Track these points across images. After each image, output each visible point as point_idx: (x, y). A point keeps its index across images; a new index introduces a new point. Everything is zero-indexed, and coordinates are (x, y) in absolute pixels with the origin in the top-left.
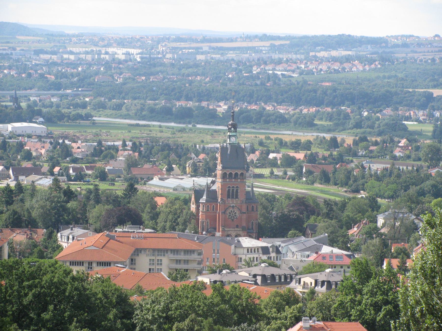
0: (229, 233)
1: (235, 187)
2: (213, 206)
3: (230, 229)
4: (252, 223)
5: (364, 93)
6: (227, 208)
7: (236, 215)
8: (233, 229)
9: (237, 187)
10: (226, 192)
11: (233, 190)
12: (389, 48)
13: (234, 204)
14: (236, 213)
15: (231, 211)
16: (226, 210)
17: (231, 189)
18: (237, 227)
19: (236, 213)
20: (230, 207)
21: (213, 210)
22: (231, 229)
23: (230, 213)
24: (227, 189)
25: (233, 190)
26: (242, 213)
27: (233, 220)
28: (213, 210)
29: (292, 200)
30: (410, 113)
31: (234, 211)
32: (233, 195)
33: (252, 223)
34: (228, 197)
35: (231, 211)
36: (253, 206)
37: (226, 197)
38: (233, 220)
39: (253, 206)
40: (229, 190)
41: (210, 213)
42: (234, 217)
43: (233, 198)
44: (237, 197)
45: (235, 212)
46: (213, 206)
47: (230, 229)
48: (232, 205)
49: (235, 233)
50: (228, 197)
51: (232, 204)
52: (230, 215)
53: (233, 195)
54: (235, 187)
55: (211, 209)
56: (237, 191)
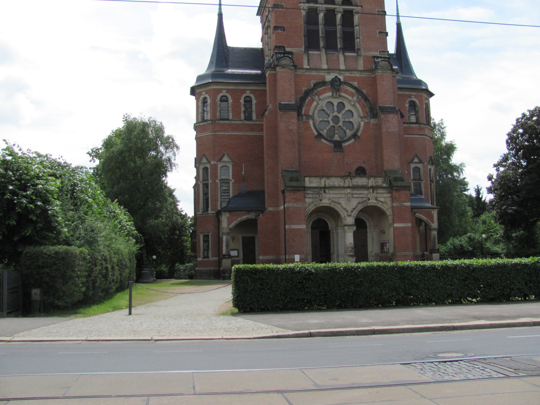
0: (325, 202)
2: (248, 101)
5: (2, 316)
6: (308, 93)
10: (301, 21)
12: (248, 90)
16: (303, 99)
18: (361, 172)
20: (324, 83)
21: (248, 118)
22: (336, 182)
26: (374, 110)
28: (248, 118)
29: (113, 149)
31: (341, 106)
32: (330, 37)
34: (312, 43)
37: (302, 40)
38: (338, 145)
40: (312, 14)
41: (236, 128)
43: (331, 46)
44: (349, 44)
45: (348, 107)
46: (248, 101)
48: (329, 77)
49: (354, 202)
50: (312, 43)
51: (329, 70)
53: (330, 37)
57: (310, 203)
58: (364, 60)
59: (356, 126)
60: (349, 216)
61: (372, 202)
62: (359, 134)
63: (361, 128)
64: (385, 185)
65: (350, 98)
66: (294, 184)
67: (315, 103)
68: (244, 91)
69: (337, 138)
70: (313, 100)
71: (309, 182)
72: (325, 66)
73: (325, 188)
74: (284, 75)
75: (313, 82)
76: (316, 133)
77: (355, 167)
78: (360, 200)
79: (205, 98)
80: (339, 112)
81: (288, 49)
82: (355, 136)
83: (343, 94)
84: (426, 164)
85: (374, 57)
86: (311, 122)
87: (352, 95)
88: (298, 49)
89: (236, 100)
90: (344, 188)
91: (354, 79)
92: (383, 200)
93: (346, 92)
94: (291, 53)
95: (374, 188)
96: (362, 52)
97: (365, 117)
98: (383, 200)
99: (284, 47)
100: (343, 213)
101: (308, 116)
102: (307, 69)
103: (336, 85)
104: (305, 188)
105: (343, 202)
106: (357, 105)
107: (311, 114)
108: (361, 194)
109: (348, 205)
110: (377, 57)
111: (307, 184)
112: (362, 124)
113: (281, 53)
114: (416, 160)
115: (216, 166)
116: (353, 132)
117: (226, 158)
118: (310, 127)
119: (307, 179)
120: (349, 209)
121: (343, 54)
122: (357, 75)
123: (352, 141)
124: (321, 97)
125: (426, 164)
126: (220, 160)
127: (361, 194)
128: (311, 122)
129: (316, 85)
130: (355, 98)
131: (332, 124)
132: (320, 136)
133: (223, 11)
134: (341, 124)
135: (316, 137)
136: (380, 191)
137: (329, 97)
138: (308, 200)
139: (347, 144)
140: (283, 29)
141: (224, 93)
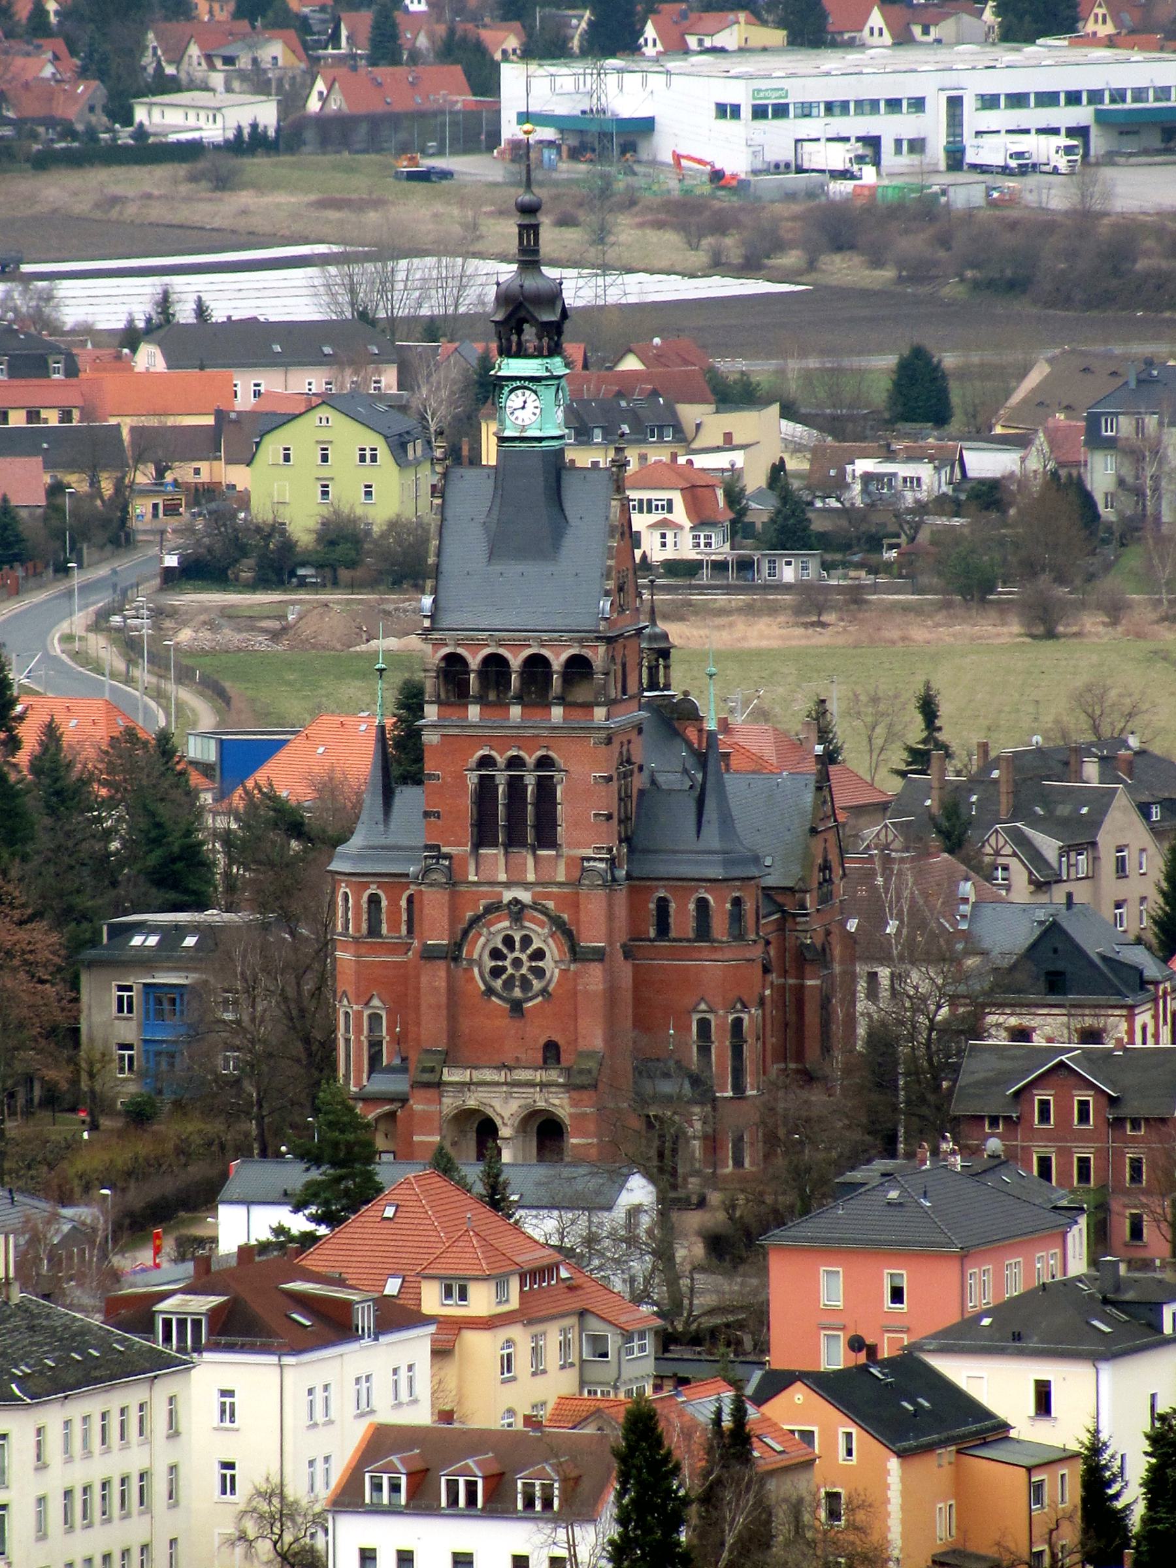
0: (472, 1103)
1: (530, 760)
3: (478, 1075)
4: (704, 1025)
6: (465, 933)
7: (540, 973)
8: (500, 1077)
9: (545, 763)
11: (516, 785)
13: (526, 885)
14: (539, 955)
15: (509, 941)
17: (501, 778)
19: (539, 955)
22: (489, 1075)
23: (496, 954)
24: (472, 779)
25: (516, 785)
26: (576, 953)
27: (517, 1007)
30: (572, 1546)
31: (526, 941)
33: (704, 1025)
34: (483, 836)
35: (509, 941)
36: (702, 904)
38: (517, 1007)
39: (702, 904)
40: (486, 786)
41: (393, 948)
42: (526, 984)
43: (514, 840)
44: (546, 836)
47: (478, 1075)
48: (508, 896)
50: (483, 836)
51: (508, 885)
52: (497, 972)
54: (530, 760)
55: (394, 926)
56: (546, 788)
57: (450, 1103)
58: (567, 865)
59: (548, 975)
60: (505, 1124)
61: (541, 1104)
62: (550, 989)
63: (555, 980)
64: (561, 1080)
65: (539, 930)
66: (426, 1077)
67: (482, 940)
68: (696, 890)
69: (517, 993)
70: (480, 935)
71: (451, 1075)
72: (503, 877)
73: (471, 1083)
74: (435, 904)
75: (482, 903)
76: (483, 987)
77: (542, 1041)
78: (522, 1102)
79: (346, 894)
80: (523, 950)
81: (444, 850)
82: (544, 991)
83: (527, 924)
84: (721, 1012)
85: (584, 859)
86: (476, 970)
87: (541, 925)
88: (460, 850)
89: (394, 902)
90: (497, 1084)
91: (548, 896)
92: (557, 1102)
93: (533, 920)
94: (448, 857)
95: (543, 1085)
96: (565, 851)
97: (562, 961)
98: (560, 1104)
99: (438, 847)
100: (498, 1122)
101: (471, 961)
102: (474, 883)
103: (517, 911)
104: (439, 1084)
105: (497, 1104)
106: (550, 940)
107: (476, 956)
108: (347, 1041)
109: (506, 1110)
110: (589, 859)
111: (446, 1077)
112: (557, 971)
113: (432, 857)
114: (703, 1007)
115: (359, 1014)
116: (543, 984)
117: (376, 1002)
118: (473, 978)
119: (445, 1070)
120: (506, 1115)
121: (534, 854)
122: (555, 890)
123: (540, 999)
124: (492, 929)
125: (721, 1012)
126: (367, 1004)
127: (347, 1041)
128: (476, 970)
129: (488, 910)
130: (546, 930)
131: (510, 971)
132: (490, 991)
133: (496, 250)
134: (524, 971)
135: (484, 993)
136: (553, 1089)
137: (505, 929)
138: (445, 1100)
139: (530, 1004)
140: (438, 815)
141: (373, 889)
